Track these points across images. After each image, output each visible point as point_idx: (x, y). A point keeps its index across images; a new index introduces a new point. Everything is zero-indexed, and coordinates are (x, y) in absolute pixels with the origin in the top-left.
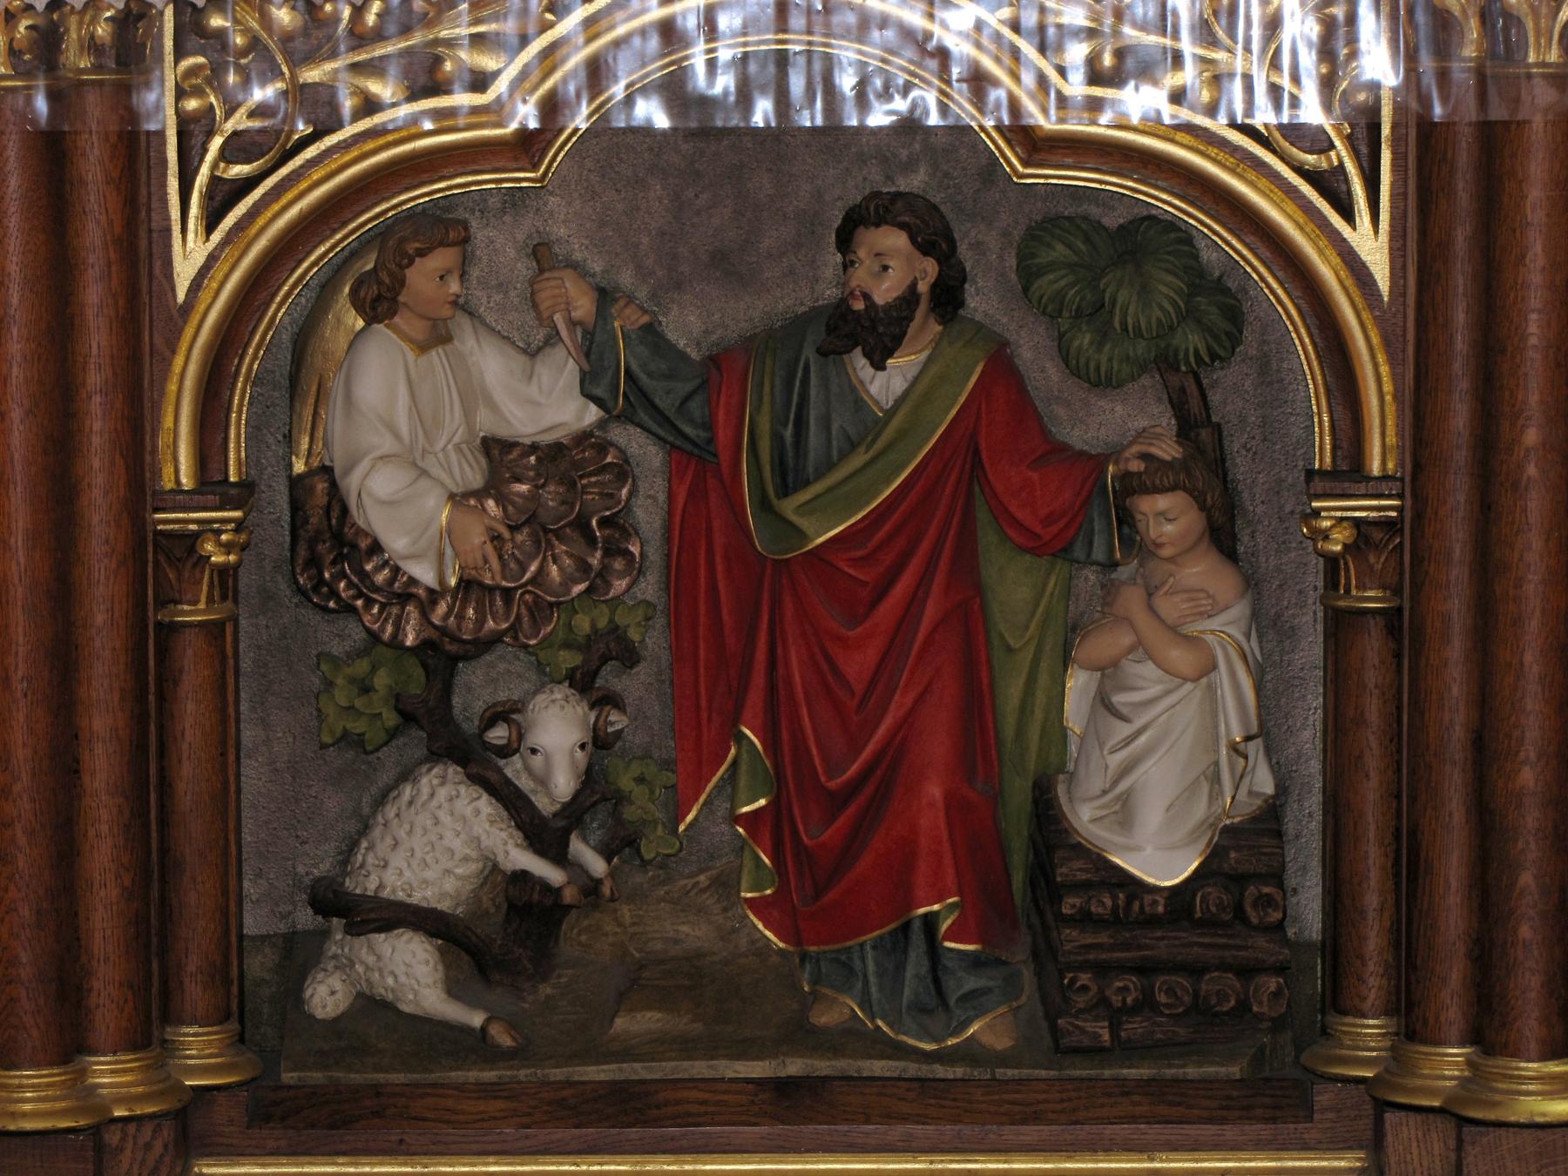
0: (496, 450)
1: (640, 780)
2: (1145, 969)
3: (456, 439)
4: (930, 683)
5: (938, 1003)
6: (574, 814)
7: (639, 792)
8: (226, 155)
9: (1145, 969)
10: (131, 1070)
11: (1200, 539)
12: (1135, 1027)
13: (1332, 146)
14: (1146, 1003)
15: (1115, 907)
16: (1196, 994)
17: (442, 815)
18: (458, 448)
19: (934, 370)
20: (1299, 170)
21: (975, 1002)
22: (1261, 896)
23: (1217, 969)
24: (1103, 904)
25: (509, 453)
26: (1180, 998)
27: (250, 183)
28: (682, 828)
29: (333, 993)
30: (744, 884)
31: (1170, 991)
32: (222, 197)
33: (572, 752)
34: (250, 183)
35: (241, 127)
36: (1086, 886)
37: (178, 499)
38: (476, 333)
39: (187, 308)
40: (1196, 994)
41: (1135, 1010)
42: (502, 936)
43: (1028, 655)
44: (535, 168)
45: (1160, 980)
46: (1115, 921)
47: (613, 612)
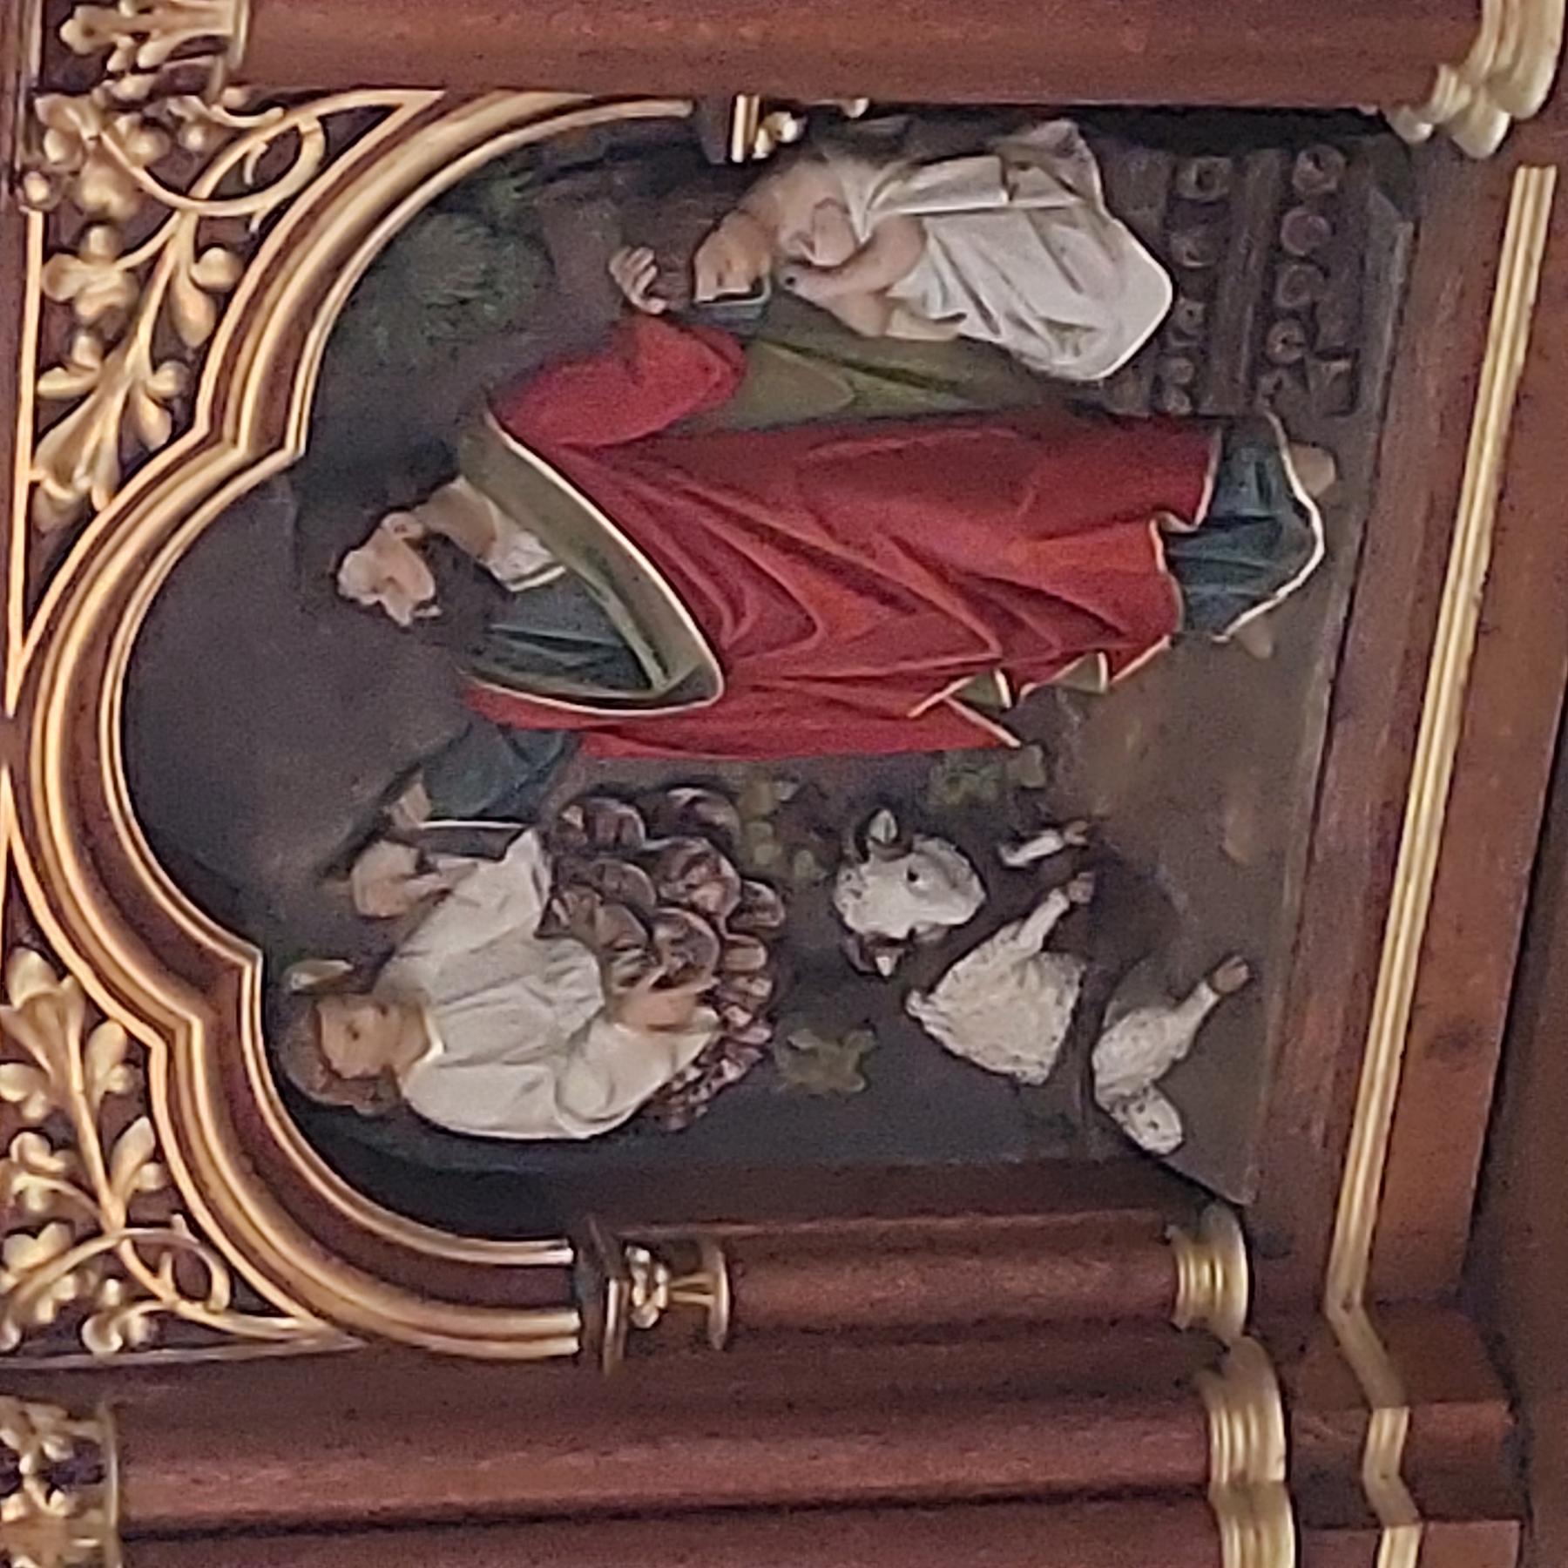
0: (548, 928)
1: (953, 781)
2: (1268, 315)
3: (539, 987)
4: (898, 541)
5: (1275, 536)
6: (988, 869)
7: (968, 783)
8: (201, 1294)
9: (1268, 315)
10: (1258, 1535)
11: (744, 212)
12: (1332, 331)
13: (295, 129)
14: (1309, 319)
15: (1186, 353)
16: (1302, 260)
17: (966, 1009)
18: (552, 979)
19: (514, 505)
20: (324, 165)
21: (1271, 487)
22: (1199, 182)
23: (1279, 233)
24: (1179, 368)
25: (557, 917)
26: (1285, 186)
27: (233, 1273)
28: (1014, 742)
29: (1155, 1125)
30: (1090, 688)
31: (1295, 291)
32: (246, 1301)
33: (921, 894)
34: (233, 1273)
35: (171, 1285)
36: (1158, 386)
37: (590, 1336)
38: (412, 954)
39: (370, 1336)
40: (1302, 260)
41: (1312, 334)
42: (1115, 952)
43: (861, 379)
44: (239, 970)
45: (1282, 301)
46: (1201, 357)
47: (756, 818)
